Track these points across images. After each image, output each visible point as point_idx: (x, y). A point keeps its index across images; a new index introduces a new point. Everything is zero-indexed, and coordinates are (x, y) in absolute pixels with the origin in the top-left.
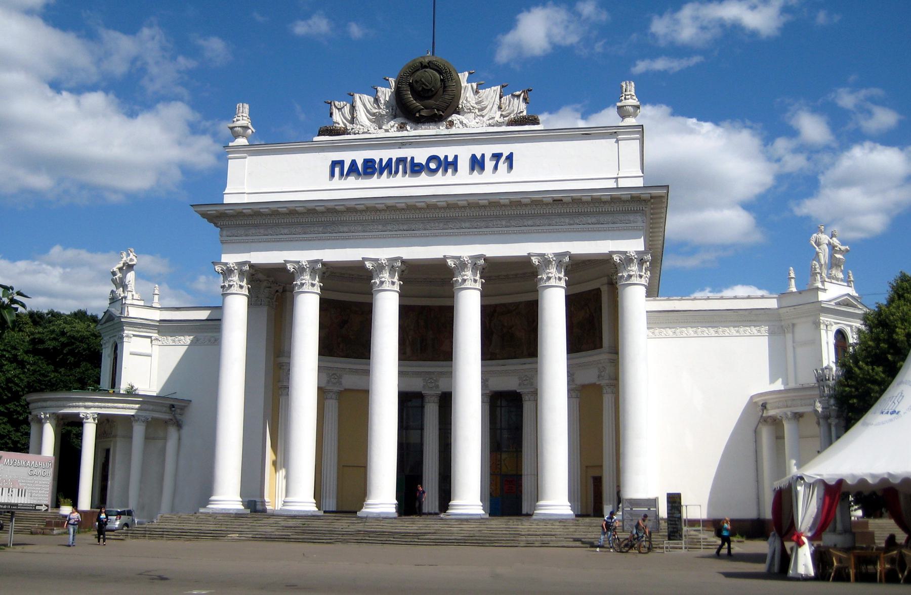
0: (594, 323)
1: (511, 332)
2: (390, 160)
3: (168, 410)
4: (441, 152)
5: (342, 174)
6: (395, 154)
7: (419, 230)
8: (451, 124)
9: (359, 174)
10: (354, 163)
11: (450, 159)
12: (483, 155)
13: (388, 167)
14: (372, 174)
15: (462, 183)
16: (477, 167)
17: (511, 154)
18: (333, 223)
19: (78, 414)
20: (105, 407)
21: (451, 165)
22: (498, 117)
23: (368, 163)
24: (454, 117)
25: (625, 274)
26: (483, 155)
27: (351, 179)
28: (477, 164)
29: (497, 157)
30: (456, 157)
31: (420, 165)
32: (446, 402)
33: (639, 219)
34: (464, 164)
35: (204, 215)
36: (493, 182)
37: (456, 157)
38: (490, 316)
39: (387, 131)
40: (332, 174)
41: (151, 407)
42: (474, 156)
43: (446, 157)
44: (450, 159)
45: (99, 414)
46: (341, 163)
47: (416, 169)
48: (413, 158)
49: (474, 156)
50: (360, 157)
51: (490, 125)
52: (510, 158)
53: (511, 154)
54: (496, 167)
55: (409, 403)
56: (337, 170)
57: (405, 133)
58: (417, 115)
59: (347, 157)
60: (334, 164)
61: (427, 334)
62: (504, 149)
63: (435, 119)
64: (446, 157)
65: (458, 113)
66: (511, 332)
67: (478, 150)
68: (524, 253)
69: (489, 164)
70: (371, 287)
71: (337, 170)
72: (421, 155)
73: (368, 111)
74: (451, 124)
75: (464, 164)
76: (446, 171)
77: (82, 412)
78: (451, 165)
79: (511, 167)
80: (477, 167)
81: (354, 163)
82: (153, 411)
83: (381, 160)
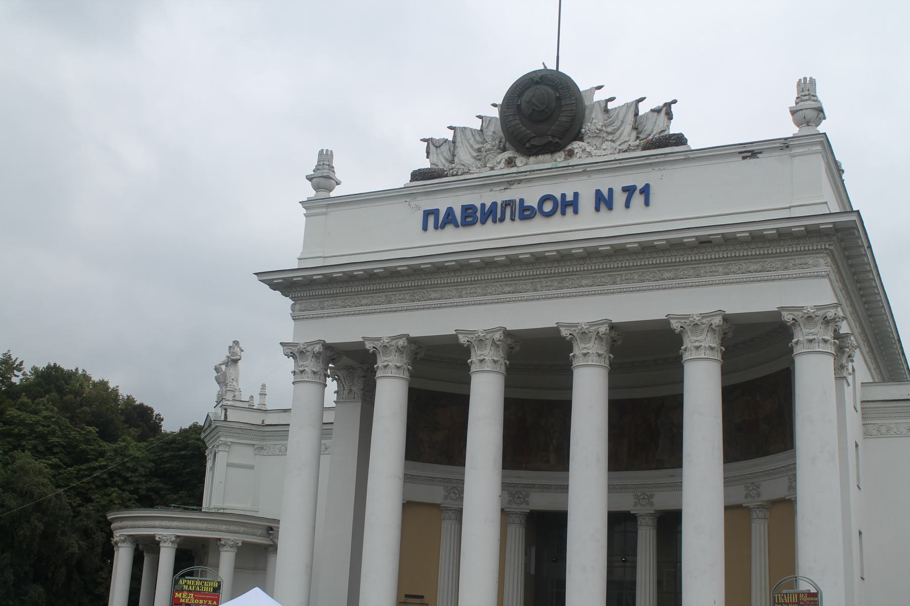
0: (761, 419)
1: (645, 433)
2: (494, 204)
3: (264, 532)
4: (557, 189)
5: (436, 227)
6: (499, 196)
7: (777, 269)
8: (571, 154)
9: (457, 226)
10: (450, 211)
11: (570, 198)
12: (611, 191)
13: (491, 214)
14: (472, 224)
15: (586, 226)
16: (603, 207)
17: (647, 186)
18: (422, 287)
19: (153, 536)
20: (197, 529)
21: (569, 205)
22: (633, 143)
23: (468, 210)
24: (576, 145)
25: (354, 388)
26: (611, 191)
27: (450, 228)
28: (603, 201)
29: (629, 190)
30: (576, 195)
31: (530, 208)
32: (670, 525)
33: (822, 261)
34: (587, 202)
35: (274, 286)
36: (627, 223)
37: (576, 195)
38: (733, 396)
39: (492, 169)
40: (425, 228)
41: (242, 529)
42: (598, 192)
43: (563, 196)
44: (570, 198)
45: (178, 537)
46: (435, 212)
47: (525, 213)
48: (522, 201)
49: (598, 192)
50: (457, 202)
51: (620, 151)
52: (646, 191)
53: (647, 186)
54: (627, 205)
55: (620, 525)
56: (431, 220)
57: (514, 170)
58: (527, 145)
59: (441, 204)
60: (427, 214)
61: (536, 435)
62: (638, 179)
63: (551, 148)
64: (563, 196)
65: (581, 140)
66: (645, 433)
67: (603, 183)
68: (772, 307)
69: (619, 199)
70: (467, 368)
71: (431, 220)
72: (531, 195)
73: (471, 146)
74: (571, 154)
75: (587, 202)
76: (563, 213)
77: (159, 533)
78: (569, 205)
79: (647, 203)
80: (603, 207)
81: (450, 211)
82: (243, 533)
83: (483, 205)
